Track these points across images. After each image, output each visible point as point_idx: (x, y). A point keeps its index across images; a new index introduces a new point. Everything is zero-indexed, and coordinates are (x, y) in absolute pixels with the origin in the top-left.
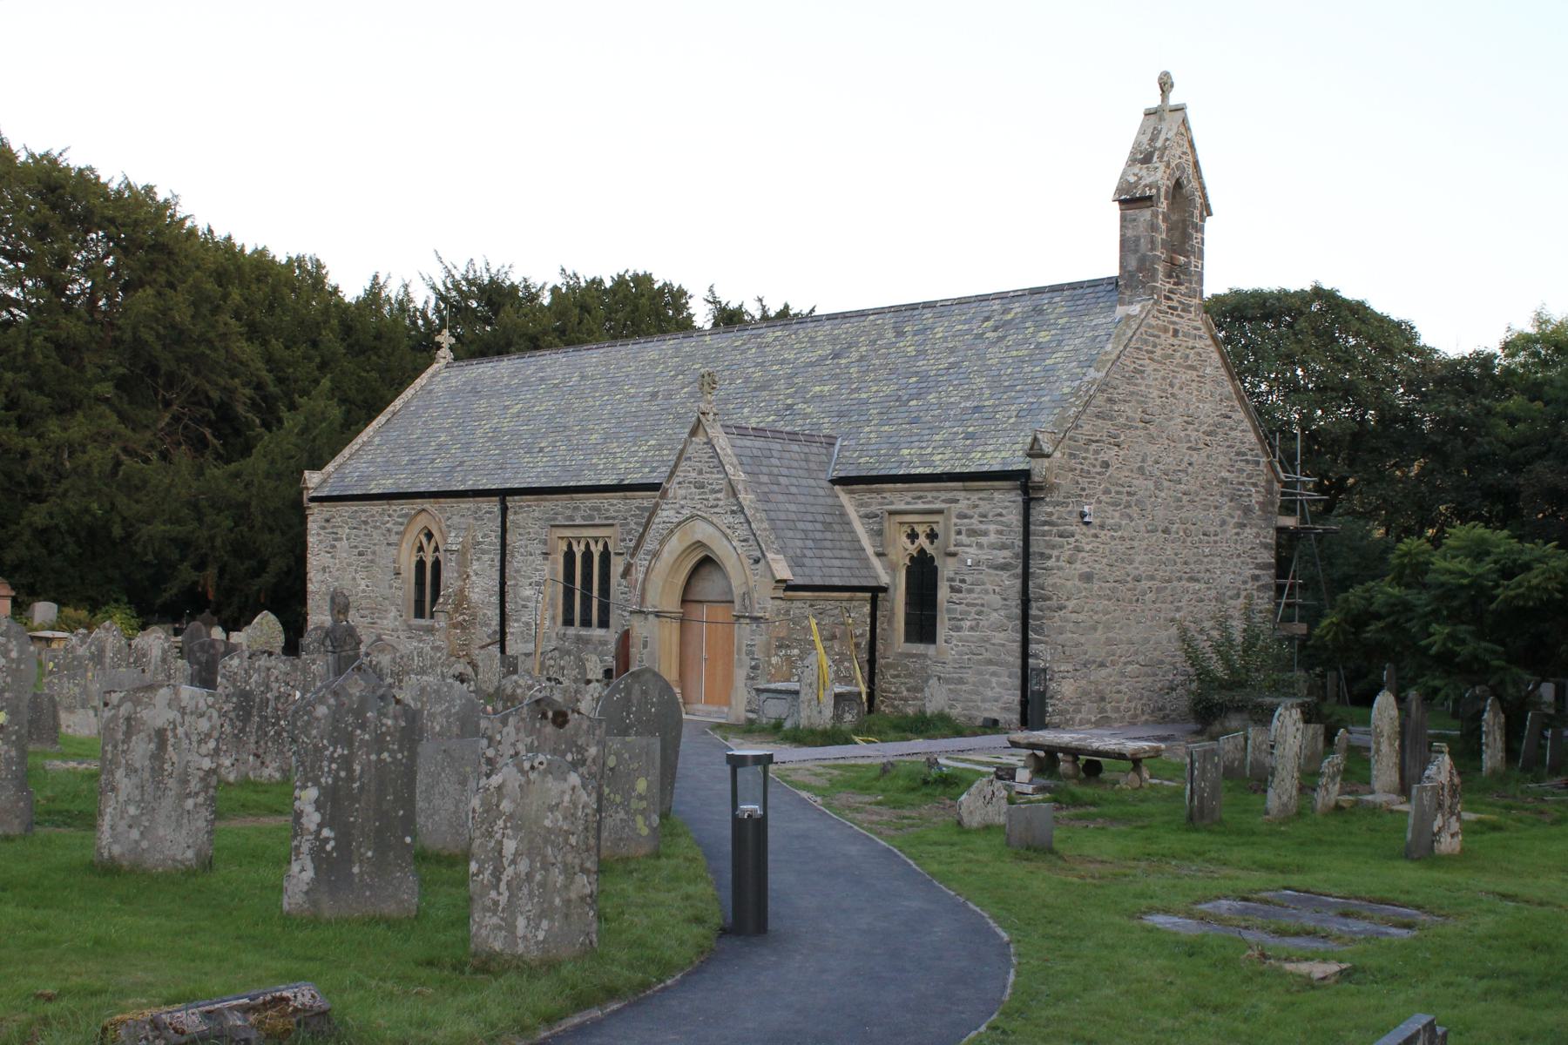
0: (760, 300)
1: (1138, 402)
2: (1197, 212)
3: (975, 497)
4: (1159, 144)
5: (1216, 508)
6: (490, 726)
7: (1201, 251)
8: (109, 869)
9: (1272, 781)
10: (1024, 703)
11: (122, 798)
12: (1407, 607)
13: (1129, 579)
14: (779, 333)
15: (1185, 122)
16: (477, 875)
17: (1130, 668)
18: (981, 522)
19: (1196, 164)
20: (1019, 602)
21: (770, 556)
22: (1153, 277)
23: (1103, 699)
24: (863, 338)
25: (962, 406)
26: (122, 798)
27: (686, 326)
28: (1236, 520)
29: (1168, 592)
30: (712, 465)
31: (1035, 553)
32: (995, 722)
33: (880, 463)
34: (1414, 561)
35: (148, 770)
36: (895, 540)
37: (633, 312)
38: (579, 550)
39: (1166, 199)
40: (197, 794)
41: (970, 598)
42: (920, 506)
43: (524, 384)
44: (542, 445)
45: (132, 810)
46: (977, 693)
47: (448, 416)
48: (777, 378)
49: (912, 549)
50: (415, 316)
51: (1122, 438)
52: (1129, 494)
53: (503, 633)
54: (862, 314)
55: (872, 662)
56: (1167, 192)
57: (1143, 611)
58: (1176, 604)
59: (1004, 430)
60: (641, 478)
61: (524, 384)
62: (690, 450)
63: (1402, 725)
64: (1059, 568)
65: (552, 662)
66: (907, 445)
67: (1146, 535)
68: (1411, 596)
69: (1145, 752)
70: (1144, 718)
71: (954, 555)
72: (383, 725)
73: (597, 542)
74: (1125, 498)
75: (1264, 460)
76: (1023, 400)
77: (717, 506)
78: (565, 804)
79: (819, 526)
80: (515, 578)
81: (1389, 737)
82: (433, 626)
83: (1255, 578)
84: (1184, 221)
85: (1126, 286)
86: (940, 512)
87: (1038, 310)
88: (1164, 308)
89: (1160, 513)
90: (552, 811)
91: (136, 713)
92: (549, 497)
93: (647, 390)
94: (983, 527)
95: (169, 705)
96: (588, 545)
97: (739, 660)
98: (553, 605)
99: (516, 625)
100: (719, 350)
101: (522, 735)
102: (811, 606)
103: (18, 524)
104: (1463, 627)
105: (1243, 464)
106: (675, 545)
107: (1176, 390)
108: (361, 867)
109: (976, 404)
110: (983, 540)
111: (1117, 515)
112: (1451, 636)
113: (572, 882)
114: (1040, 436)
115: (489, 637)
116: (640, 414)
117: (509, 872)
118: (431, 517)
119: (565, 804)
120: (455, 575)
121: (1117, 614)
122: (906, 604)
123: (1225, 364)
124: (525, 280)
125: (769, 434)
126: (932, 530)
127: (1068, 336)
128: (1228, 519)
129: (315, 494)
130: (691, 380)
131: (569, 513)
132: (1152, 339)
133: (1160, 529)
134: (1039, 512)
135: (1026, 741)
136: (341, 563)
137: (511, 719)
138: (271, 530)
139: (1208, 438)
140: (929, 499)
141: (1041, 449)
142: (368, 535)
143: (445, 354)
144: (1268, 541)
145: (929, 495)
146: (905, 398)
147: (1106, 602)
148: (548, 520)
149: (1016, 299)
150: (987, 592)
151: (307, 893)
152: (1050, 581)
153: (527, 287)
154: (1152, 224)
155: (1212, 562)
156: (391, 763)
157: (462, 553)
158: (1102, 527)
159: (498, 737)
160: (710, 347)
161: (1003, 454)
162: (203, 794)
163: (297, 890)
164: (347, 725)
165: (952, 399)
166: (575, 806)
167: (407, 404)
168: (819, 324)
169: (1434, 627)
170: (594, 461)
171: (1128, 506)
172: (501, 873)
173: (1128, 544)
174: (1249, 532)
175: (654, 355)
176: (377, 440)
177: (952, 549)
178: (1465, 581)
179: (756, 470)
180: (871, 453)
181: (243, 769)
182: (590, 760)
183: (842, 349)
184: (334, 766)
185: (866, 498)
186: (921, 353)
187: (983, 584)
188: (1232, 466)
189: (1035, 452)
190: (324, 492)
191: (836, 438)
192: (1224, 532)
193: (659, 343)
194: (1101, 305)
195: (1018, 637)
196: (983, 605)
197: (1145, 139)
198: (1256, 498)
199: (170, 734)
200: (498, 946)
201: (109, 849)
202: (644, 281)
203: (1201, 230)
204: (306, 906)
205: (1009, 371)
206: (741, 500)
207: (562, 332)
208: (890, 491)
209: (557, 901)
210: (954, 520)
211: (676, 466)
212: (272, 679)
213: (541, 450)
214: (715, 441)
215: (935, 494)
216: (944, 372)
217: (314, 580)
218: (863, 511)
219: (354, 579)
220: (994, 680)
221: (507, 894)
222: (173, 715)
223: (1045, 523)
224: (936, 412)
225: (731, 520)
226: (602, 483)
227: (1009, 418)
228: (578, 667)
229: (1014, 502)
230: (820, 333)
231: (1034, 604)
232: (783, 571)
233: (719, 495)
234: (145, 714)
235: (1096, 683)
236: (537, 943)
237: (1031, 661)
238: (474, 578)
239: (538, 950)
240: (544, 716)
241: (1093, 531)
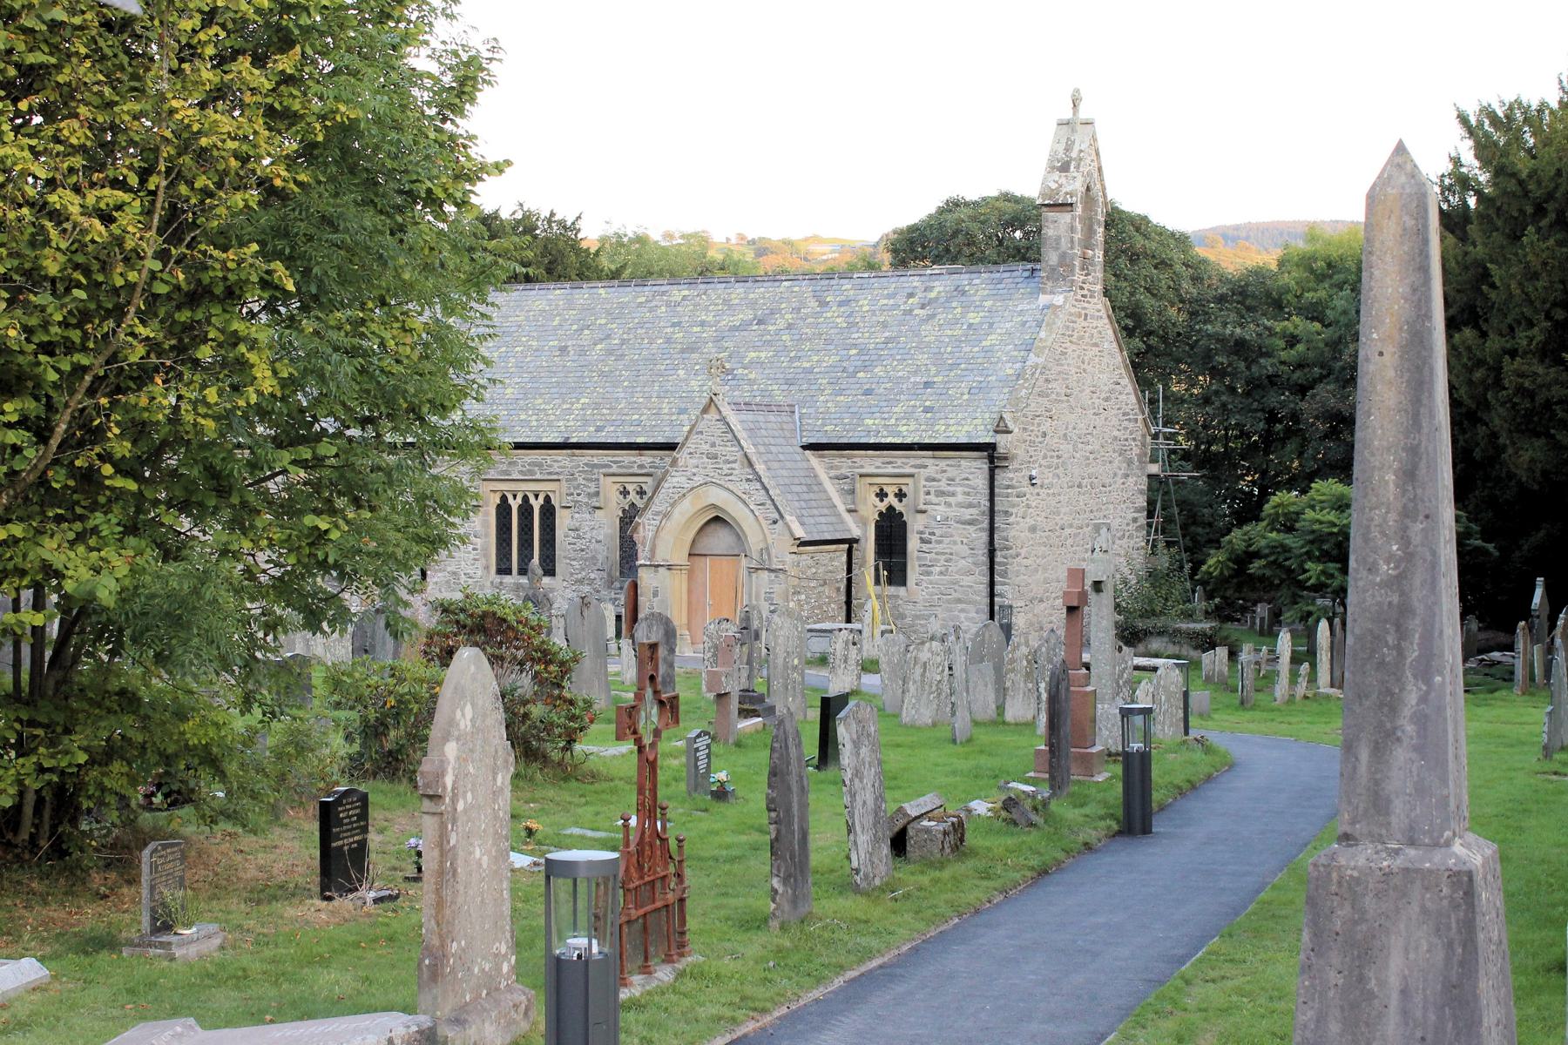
1: (1064, 379)
3: (943, 464)
12: (1286, 549)
19: (1100, 169)
21: (788, 518)
22: (1072, 272)
25: (912, 380)
38: (515, 504)
41: (939, 548)
42: (890, 470)
49: (883, 507)
52: (1058, 457)
55: (848, 603)
59: (960, 405)
62: (701, 426)
63: (1332, 642)
68: (1289, 540)
71: (924, 512)
73: (515, 497)
74: (1055, 460)
75: (1140, 417)
76: (971, 378)
79: (805, 488)
83: (1135, 520)
84: (1090, 219)
86: (911, 476)
88: (1079, 297)
94: (950, 488)
96: (525, 498)
100: (622, 306)
104: (1331, 565)
106: (686, 508)
107: (1085, 366)
109: (925, 379)
110: (950, 499)
112: (1323, 572)
126: (900, 490)
134: (1002, 478)
145: (899, 461)
146: (851, 370)
150: (955, 543)
152: (1012, 533)
155: (1107, 509)
165: (900, 374)
169: (1309, 565)
174: (1131, 480)
178: (1335, 530)
185: (836, 462)
186: (851, 325)
187: (952, 536)
195: (986, 580)
197: (1061, 148)
198: (1136, 451)
205: (949, 349)
208: (861, 456)
215: (904, 460)
218: (833, 473)
220: (963, 615)
223: (1008, 487)
224: (888, 385)
227: (962, 394)
230: (733, 296)
231: (998, 553)
232: (800, 533)
233: (733, 465)
234: (920, 655)
237: (996, 599)
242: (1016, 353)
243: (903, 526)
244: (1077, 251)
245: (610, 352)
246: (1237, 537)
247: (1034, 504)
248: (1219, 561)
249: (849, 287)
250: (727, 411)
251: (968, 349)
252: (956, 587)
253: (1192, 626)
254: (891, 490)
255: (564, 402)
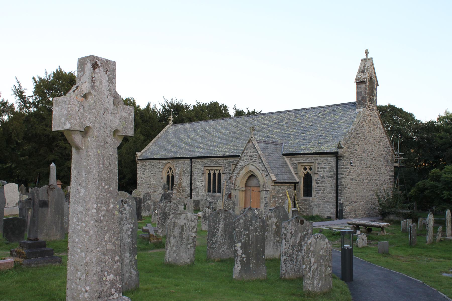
0: (248, 109)
1: (363, 134)
2: (375, 85)
3: (322, 159)
4: (366, 68)
5: (381, 161)
6: (285, 225)
7: (376, 95)
8: (170, 265)
9: (428, 234)
10: (337, 212)
11: (172, 245)
12: (436, 187)
13: (361, 180)
14: (263, 117)
15: (372, 62)
16: (305, 269)
17: (361, 203)
18: (324, 165)
19: (375, 73)
20: (335, 186)
21: (270, 174)
22: (366, 102)
23: (355, 211)
24: (286, 118)
25: (316, 135)
26: (172, 245)
27: (227, 115)
28: (385, 164)
29: (370, 183)
30: (254, 151)
31: (339, 173)
32: (330, 217)
33: (296, 150)
34: (436, 175)
35: (179, 237)
36: (300, 170)
37: (215, 112)
38: (212, 173)
39: (368, 82)
40: (191, 244)
42: (307, 161)
43: (193, 130)
44: (201, 146)
45: (174, 248)
46: (324, 210)
47: (174, 138)
48: (263, 128)
49: (305, 172)
50: (157, 113)
51: (359, 143)
52: (361, 158)
53: (191, 194)
54: (285, 112)
56: (368, 80)
57: (364, 188)
58: (372, 186)
59: (329, 141)
60: (229, 154)
61: (193, 130)
62: (248, 147)
64: (346, 177)
65: (227, 203)
66: (302, 145)
67: (365, 168)
68: (437, 184)
69: (386, 226)
70: (365, 216)
71: (317, 174)
72: (256, 225)
73: (217, 171)
74: (360, 159)
75: (391, 149)
76: (333, 134)
77: (255, 161)
78: (325, 248)
79: (281, 166)
80: (194, 180)
81: (449, 222)
82: (172, 193)
83: (390, 179)
84: (372, 87)
85: (358, 104)
86: (313, 163)
87: (334, 111)
88: (368, 110)
89: (368, 163)
90: (322, 250)
91: (176, 221)
92: (204, 159)
93: (228, 131)
95: (185, 219)
96: (214, 172)
97: (262, 201)
98: (205, 187)
99: (195, 192)
100: (246, 121)
101: (293, 227)
102: (280, 187)
103: (64, 166)
105: (386, 150)
106: (244, 171)
107: (371, 131)
108: (252, 265)
109: (320, 135)
110: (325, 170)
111: (358, 163)
112: (449, 194)
113: (327, 270)
114: (341, 143)
115: (187, 195)
116: (227, 137)
117: (313, 267)
118: (171, 164)
119: (325, 248)
120: (178, 179)
121: (358, 189)
122: (303, 187)
123: (382, 124)
124: (186, 104)
125: (267, 143)
126: (310, 167)
127: (343, 117)
128: (383, 164)
129: (139, 158)
130: (240, 129)
131: (209, 163)
132: (366, 118)
133: (368, 167)
134: (340, 163)
135: (352, 223)
136: (146, 176)
137: (290, 223)
138: (127, 168)
139: (379, 143)
140: (310, 159)
141: (341, 146)
142: (154, 169)
143: (171, 122)
144: (392, 170)
145: (310, 158)
146: (300, 133)
147: (356, 186)
148: (203, 165)
149: (327, 108)
150: (326, 183)
151: (239, 273)
152: (343, 180)
153: (186, 105)
154: (365, 88)
156: (259, 235)
157: (180, 173)
158: (355, 166)
159: (287, 228)
160: (244, 120)
161: (330, 148)
162: (192, 244)
163: (237, 272)
164: (248, 225)
165: (313, 133)
166: (327, 248)
167: (162, 135)
168: (273, 114)
169: (444, 192)
170: (216, 150)
171: (361, 161)
172: (311, 268)
173: (361, 171)
174: (388, 167)
175: (229, 122)
176: (155, 144)
177: (316, 172)
179: (265, 152)
180: (293, 147)
181: (164, 233)
182: (309, 233)
183: (280, 121)
184: (245, 237)
185: (292, 159)
186: (303, 122)
187: (325, 181)
188: (384, 150)
189: (339, 147)
190: (142, 158)
191: (283, 144)
192: (382, 167)
193: (229, 119)
194: (351, 109)
195: (335, 195)
196: (325, 187)
197: (362, 67)
198: (390, 159)
199: (184, 227)
200: (310, 289)
201: (169, 259)
202: (216, 104)
203: (376, 90)
204: (239, 277)
205: (328, 126)
206: (262, 160)
207: (197, 117)
209: (323, 275)
210: (317, 165)
211: (244, 151)
212: (171, 209)
213: (200, 147)
214: (255, 144)
216: (310, 126)
217: (139, 180)
218: (291, 162)
219: (150, 180)
220: (328, 206)
221: (312, 274)
222: (185, 221)
223: (342, 165)
224: (309, 137)
225: (260, 165)
226: (219, 155)
227: (330, 138)
228: (233, 204)
229: (333, 160)
230: (274, 117)
231: (339, 187)
232: (274, 178)
233: (256, 159)
234: (178, 221)
235: (354, 207)
236: (319, 288)
237: (339, 201)
238: (183, 180)
239: (319, 290)
240: (298, 222)
241: (353, 167)
242: (347, 126)
243: (311, 178)
244: (367, 96)
245: (240, 133)
246: (420, 183)
247: (352, 172)
248: (414, 191)
249: (304, 112)
250: (255, 142)
251: (334, 126)
252: (326, 197)
253: (404, 211)
254: (307, 167)
255: (226, 145)
